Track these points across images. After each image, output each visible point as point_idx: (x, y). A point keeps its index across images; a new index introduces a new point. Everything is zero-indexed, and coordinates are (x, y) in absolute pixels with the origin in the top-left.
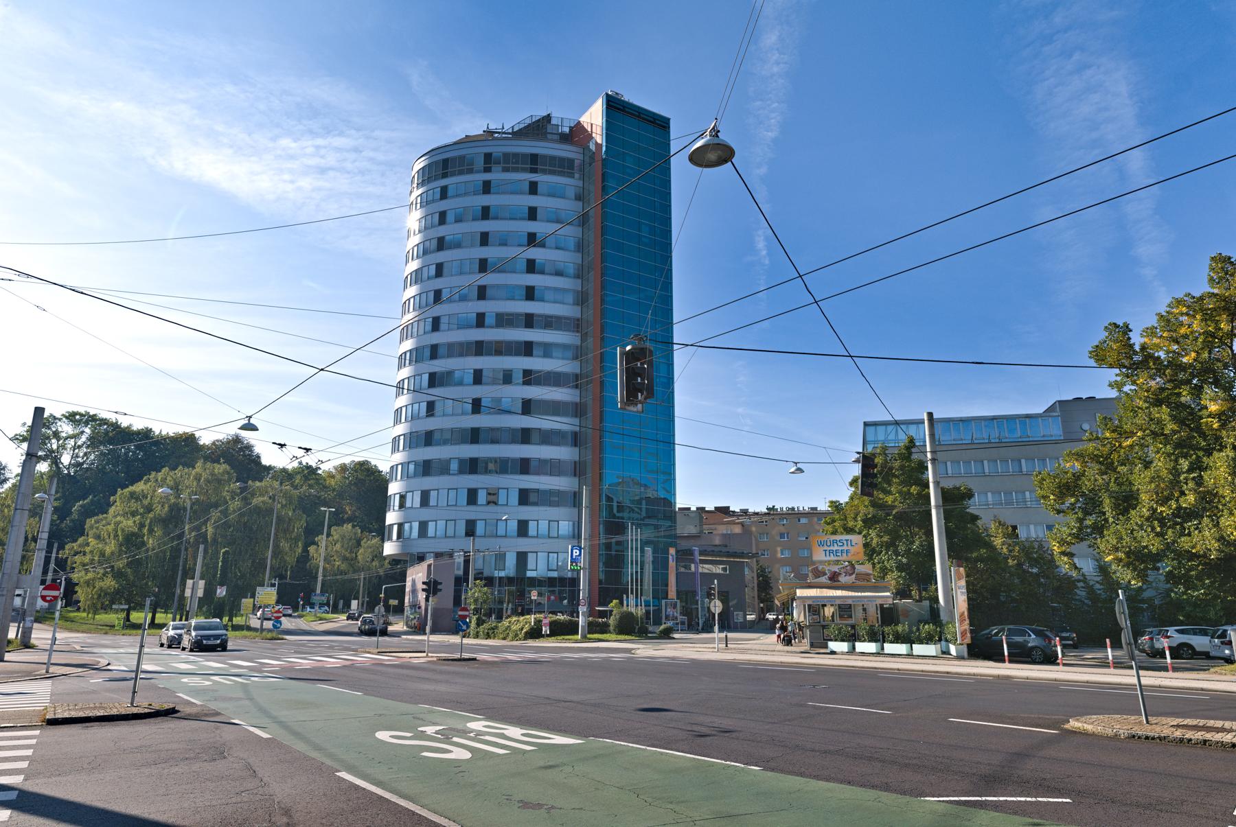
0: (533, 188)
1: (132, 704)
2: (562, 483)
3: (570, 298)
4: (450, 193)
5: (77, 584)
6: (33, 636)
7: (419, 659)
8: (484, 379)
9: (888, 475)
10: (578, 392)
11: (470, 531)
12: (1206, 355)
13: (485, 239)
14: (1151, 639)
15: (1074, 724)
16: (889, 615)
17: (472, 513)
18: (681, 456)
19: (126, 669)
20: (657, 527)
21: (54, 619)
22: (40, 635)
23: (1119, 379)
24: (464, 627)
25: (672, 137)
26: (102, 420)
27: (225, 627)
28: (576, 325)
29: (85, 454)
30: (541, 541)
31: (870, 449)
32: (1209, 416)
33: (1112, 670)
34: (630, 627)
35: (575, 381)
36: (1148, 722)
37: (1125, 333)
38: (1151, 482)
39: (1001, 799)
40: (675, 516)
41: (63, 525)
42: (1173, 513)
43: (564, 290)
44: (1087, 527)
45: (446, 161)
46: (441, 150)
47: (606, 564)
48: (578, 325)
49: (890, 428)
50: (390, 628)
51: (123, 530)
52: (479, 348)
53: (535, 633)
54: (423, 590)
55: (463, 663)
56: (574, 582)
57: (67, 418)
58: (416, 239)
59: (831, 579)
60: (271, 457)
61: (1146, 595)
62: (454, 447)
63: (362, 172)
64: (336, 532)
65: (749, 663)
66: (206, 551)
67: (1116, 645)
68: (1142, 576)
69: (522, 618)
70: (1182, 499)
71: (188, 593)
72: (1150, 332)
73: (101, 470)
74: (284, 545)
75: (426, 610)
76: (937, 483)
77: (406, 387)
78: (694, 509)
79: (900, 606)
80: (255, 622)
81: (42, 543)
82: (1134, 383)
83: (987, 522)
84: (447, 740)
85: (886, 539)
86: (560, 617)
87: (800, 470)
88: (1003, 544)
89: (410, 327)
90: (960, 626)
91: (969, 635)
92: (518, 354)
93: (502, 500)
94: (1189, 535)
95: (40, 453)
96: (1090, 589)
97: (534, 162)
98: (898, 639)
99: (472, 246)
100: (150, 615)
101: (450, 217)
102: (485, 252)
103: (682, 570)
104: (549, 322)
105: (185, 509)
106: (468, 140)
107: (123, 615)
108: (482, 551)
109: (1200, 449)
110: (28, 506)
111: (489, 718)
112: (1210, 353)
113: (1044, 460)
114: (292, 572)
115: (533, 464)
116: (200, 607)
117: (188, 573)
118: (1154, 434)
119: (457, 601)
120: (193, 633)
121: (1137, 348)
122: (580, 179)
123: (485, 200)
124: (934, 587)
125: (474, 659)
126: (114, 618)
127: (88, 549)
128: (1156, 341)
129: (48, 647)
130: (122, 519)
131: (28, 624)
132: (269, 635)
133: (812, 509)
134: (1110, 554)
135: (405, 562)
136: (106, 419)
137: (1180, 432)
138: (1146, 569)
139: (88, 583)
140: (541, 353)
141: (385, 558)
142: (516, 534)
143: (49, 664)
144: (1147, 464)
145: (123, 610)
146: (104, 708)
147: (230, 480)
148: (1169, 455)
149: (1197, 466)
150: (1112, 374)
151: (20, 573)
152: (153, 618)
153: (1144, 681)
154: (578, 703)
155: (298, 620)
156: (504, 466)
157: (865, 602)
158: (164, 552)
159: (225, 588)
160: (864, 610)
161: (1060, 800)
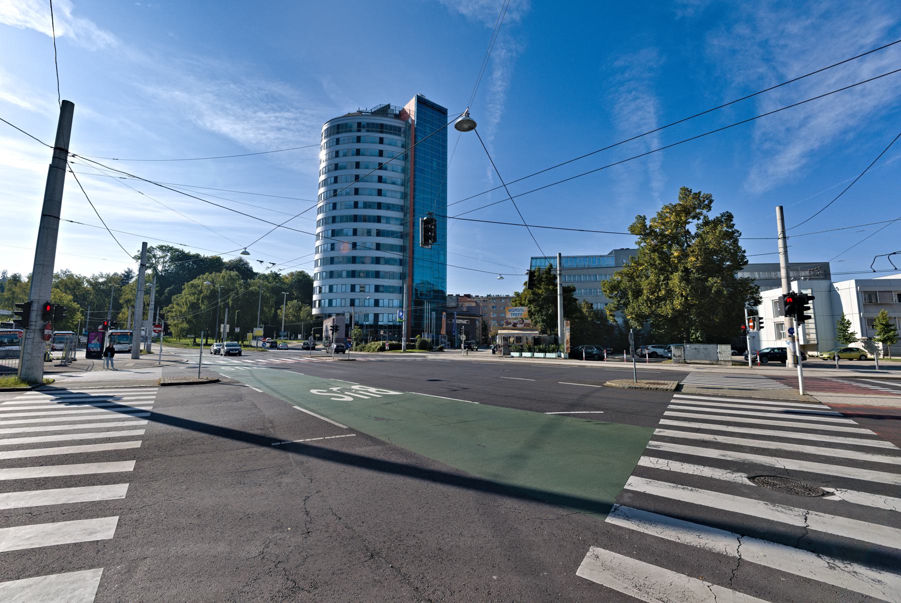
0: (381, 141)
1: (199, 377)
2: (396, 283)
3: (399, 195)
5: (169, 325)
9: (540, 280)
11: (352, 303)
12: (675, 231)
13: (358, 165)
14: (642, 350)
15: (608, 383)
16: (537, 341)
17: (353, 295)
19: (195, 363)
20: (437, 303)
22: (155, 348)
23: (639, 240)
24: (350, 346)
27: (240, 346)
28: (402, 209)
29: (169, 266)
31: (533, 269)
32: (674, 258)
33: (625, 363)
34: (425, 347)
35: (402, 236)
36: (636, 382)
37: (644, 220)
38: (648, 285)
39: (576, 412)
41: (161, 299)
42: (655, 298)
43: (396, 191)
44: (621, 304)
45: (338, 126)
47: (415, 319)
49: (542, 260)
50: (316, 347)
51: (189, 301)
52: (355, 219)
53: (382, 349)
54: (331, 330)
55: (349, 361)
56: (400, 327)
57: (159, 248)
58: (323, 165)
59: (513, 326)
60: (257, 268)
61: (642, 332)
63: (299, 131)
64: (290, 304)
65: (476, 361)
67: (628, 353)
68: (641, 324)
69: (376, 343)
71: (222, 330)
72: (654, 220)
73: (177, 273)
74: (266, 309)
76: (561, 285)
78: (454, 295)
80: (254, 343)
81: (152, 306)
82: (645, 242)
83: (581, 302)
84: (342, 393)
85: (538, 309)
86: (394, 342)
87: (502, 278)
88: (587, 311)
89: (322, 207)
90: (566, 346)
91: (569, 349)
92: (374, 221)
93: (367, 290)
94: (661, 307)
95: (147, 265)
96: (620, 330)
97: (382, 128)
98: (540, 351)
99: (351, 168)
100: (205, 340)
101: (341, 154)
103: (449, 322)
104: (389, 207)
105: (218, 292)
106: (349, 115)
107: (193, 340)
108: (358, 313)
109: (668, 271)
110: (143, 289)
111: (361, 384)
112: (676, 230)
113: (606, 275)
115: (381, 274)
116: (228, 336)
117: (222, 322)
119: (347, 335)
120: (226, 348)
121: (648, 227)
125: (355, 360)
126: (189, 341)
127: (173, 310)
128: (656, 224)
129: (159, 353)
130: (189, 296)
131: (149, 343)
132: (261, 349)
134: (629, 316)
135: (323, 317)
136: (177, 249)
138: (643, 321)
139: (175, 325)
141: (313, 316)
142: (373, 305)
143: (160, 360)
144: (647, 277)
146: (186, 379)
147: (239, 279)
148: (656, 274)
149: (667, 279)
150: (637, 238)
152: (207, 341)
153: (637, 367)
154: (401, 378)
156: (368, 274)
157: (527, 335)
158: (210, 311)
159: (239, 328)
160: (527, 339)
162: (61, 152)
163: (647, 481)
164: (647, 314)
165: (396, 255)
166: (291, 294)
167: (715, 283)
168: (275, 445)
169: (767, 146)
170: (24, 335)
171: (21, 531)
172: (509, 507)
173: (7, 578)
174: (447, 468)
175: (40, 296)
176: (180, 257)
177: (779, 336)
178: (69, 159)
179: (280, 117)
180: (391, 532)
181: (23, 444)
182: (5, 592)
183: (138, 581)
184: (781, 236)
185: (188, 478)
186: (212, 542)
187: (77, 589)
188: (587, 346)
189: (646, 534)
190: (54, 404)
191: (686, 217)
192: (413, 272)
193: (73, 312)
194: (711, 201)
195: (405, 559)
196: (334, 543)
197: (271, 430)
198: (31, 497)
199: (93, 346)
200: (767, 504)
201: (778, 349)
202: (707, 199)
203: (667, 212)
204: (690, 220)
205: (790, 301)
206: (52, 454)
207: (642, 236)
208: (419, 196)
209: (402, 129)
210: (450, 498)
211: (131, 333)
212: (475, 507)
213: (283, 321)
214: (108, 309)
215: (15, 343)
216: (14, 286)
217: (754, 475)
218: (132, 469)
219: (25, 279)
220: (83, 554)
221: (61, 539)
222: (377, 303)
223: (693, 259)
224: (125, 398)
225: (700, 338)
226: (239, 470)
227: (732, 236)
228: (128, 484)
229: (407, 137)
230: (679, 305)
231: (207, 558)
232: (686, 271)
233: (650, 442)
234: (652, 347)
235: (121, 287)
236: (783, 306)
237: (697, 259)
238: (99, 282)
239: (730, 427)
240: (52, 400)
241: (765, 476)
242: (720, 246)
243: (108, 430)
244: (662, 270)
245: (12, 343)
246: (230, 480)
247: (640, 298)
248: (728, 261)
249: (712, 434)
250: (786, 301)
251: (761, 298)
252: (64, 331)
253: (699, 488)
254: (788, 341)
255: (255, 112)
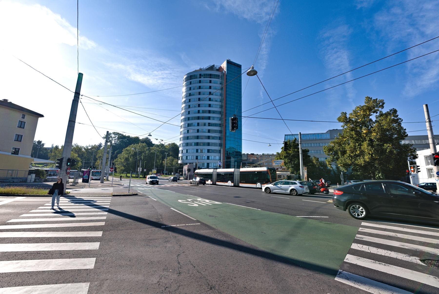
0: (210, 82)
1: (129, 192)
2: (217, 148)
3: (219, 107)
4: (192, 83)
6: (109, 178)
7: (186, 185)
8: (200, 125)
10: (220, 128)
11: (197, 158)
13: (200, 93)
16: (289, 178)
17: (197, 154)
18: (243, 142)
20: (238, 158)
21: (113, 175)
22: (110, 178)
23: (343, 125)
25: (242, 69)
26: (120, 134)
28: (220, 113)
29: (117, 141)
30: (212, 160)
31: (286, 141)
32: (363, 134)
35: (220, 125)
37: (345, 114)
38: (350, 148)
39: (313, 217)
40: (242, 155)
42: (354, 155)
43: (217, 105)
44: (335, 158)
45: (191, 76)
46: (189, 74)
48: (220, 113)
49: (291, 136)
50: (180, 179)
51: (125, 157)
52: (198, 118)
54: (187, 171)
57: (113, 133)
58: (184, 94)
60: (154, 142)
61: (347, 173)
62: (193, 140)
63: (172, 79)
64: (168, 158)
66: (142, 162)
68: (347, 169)
70: (356, 152)
71: (138, 170)
72: (351, 114)
73: (120, 144)
74: (158, 161)
75: (188, 175)
76: (301, 148)
77: (183, 126)
78: (246, 154)
79: (292, 176)
81: (110, 159)
82: (347, 126)
83: (312, 157)
84: (193, 202)
85: (289, 161)
87: (270, 145)
88: (315, 162)
89: (183, 113)
92: (207, 119)
93: (204, 152)
94: (357, 160)
96: (334, 172)
97: (211, 76)
99: (197, 95)
101: (192, 88)
102: (200, 96)
104: (214, 112)
106: (196, 71)
107: (126, 174)
114: (159, 166)
115: (210, 144)
116: (141, 173)
117: (138, 166)
118: (351, 138)
121: (348, 118)
122: (221, 79)
123: (200, 85)
124: (299, 171)
127: (118, 161)
128: (352, 116)
129: (112, 181)
131: (108, 176)
133: (273, 154)
137: (356, 137)
138: (347, 168)
139: (118, 168)
140: (212, 119)
141: (179, 164)
142: (207, 159)
143: (112, 184)
144: (349, 144)
145: (126, 174)
146: (123, 193)
149: (360, 145)
150: (342, 124)
151: (106, 165)
154: (221, 195)
155: (161, 176)
156: (204, 144)
157: (284, 175)
160: (284, 176)
161: (326, 217)
162: (77, 94)
163: (357, 258)
164: (349, 164)
165: (217, 135)
166: (169, 153)
167: (388, 147)
168: (163, 227)
169: (415, 71)
170: (60, 172)
171: (57, 262)
172: (280, 267)
173: (52, 283)
174: (247, 244)
175: (66, 155)
176: (122, 137)
177: (430, 176)
178: (80, 97)
179: (164, 73)
180: (220, 276)
181: (58, 221)
182: (52, 289)
183: (104, 291)
184: (427, 121)
185: (125, 241)
186: (136, 274)
187: (79, 292)
188: (316, 180)
189: (359, 289)
190: (69, 203)
191: (370, 112)
192: (225, 143)
193: (78, 161)
194: (383, 103)
195: (228, 292)
196: (192, 280)
197: (161, 219)
198: (61, 246)
199: (85, 177)
200: (435, 278)
201: (431, 183)
202: (381, 102)
203: (358, 110)
204: (372, 114)
205: (437, 157)
206: (69, 226)
207: (345, 123)
208: (228, 106)
209: (220, 76)
210: (249, 260)
211: (101, 171)
212: (262, 266)
213: (165, 166)
214: (91, 161)
215: (55, 175)
216: (56, 150)
217: (424, 259)
218: (101, 236)
219: (60, 148)
220: (81, 275)
221: (73, 267)
222: (208, 158)
223: (375, 134)
224: (98, 201)
225: (381, 177)
226: (147, 239)
227: (398, 121)
228: (100, 243)
229: (222, 79)
230: (368, 159)
231: (134, 282)
232: (371, 140)
233: (357, 235)
234: (353, 181)
235: (97, 151)
236: (433, 160)
237: (377, 134)
238: (88, 149)
239: (405, 229)
240: (69, 201)
241: (432, 260)
242: (390, 127)
243: (91, 216)
244: (357, 140)
245: (54, 175)
246: (143, 244)
247: (345, 155)
248: (395, 135)
249: (394, 232)
250: (435, 157)
251: (417, 155)
252: (74, 170)
253: (389, 264)
254: (437, 180)
255: (153, 72)
